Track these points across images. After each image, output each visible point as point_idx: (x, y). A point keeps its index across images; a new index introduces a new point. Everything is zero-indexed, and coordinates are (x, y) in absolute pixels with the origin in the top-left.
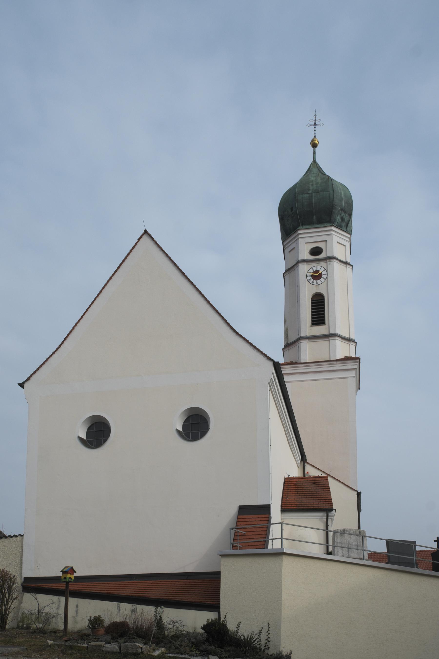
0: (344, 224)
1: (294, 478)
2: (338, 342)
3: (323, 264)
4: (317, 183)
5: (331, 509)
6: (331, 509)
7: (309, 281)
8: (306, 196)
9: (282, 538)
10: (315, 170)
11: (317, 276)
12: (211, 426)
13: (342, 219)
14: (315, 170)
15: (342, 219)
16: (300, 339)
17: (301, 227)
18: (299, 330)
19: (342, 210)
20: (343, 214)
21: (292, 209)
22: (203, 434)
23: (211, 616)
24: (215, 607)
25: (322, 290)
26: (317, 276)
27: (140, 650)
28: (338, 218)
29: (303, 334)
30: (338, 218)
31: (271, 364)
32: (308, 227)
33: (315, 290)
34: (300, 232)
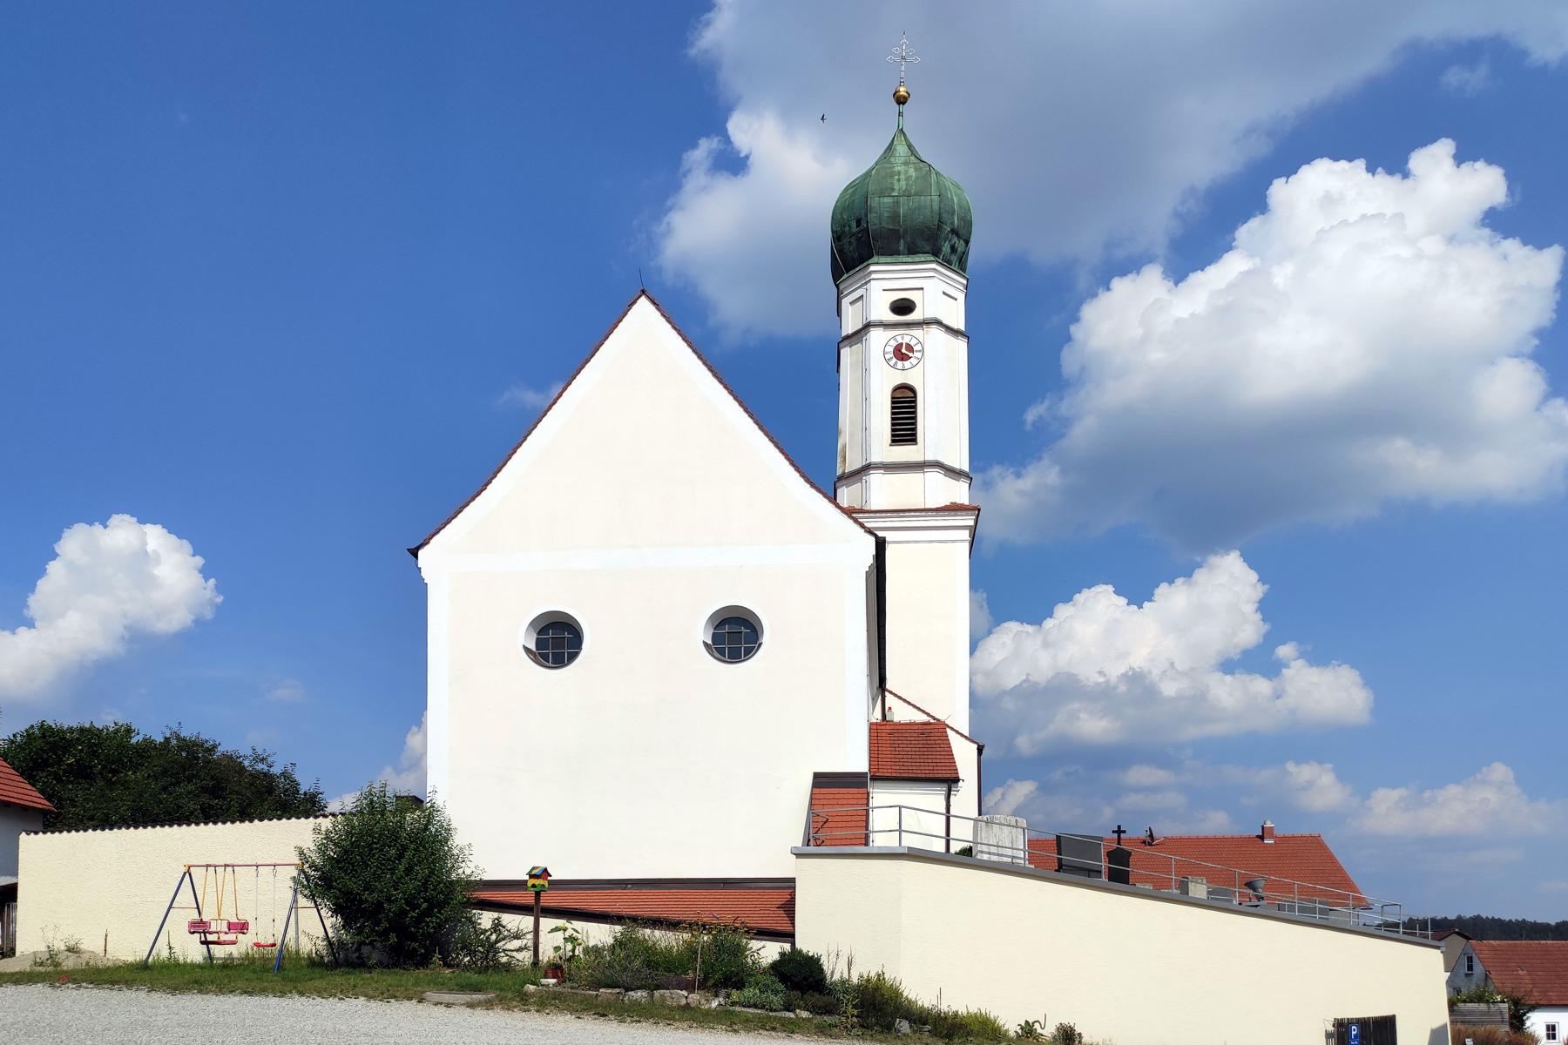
0: (954, 258)
1: (171, 530)
2: (935, 476)
3: (917, 332)
4: (908, 178)
5: (957, 780)
6: (957, 780)
7: (888, 361)
8: (887, 200)
9: (900, 831)
10: (901, 149)
11: (901, 353)
12: (766, 639)
13: (953, 249)
14: (901, 149)
15: (953, 249)
16: (867, 468)
17: (875, 259)
18: (865, 448)
19: (954, 232)
20: (955, 239)
21: (859, 222)
22: (750, 653)
23: (787, 947)
24: (789, 936)
25: (912, 378)
26: (901, 353)
27: (684, 1002)
28: (946, 248)
29: (875, 458)
30: (946, 248)
31: (872, 540)
32: (889, 259)
33: (899, 378)
34: (872, 268)
